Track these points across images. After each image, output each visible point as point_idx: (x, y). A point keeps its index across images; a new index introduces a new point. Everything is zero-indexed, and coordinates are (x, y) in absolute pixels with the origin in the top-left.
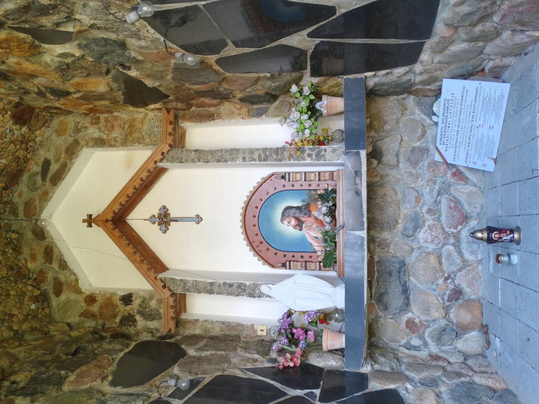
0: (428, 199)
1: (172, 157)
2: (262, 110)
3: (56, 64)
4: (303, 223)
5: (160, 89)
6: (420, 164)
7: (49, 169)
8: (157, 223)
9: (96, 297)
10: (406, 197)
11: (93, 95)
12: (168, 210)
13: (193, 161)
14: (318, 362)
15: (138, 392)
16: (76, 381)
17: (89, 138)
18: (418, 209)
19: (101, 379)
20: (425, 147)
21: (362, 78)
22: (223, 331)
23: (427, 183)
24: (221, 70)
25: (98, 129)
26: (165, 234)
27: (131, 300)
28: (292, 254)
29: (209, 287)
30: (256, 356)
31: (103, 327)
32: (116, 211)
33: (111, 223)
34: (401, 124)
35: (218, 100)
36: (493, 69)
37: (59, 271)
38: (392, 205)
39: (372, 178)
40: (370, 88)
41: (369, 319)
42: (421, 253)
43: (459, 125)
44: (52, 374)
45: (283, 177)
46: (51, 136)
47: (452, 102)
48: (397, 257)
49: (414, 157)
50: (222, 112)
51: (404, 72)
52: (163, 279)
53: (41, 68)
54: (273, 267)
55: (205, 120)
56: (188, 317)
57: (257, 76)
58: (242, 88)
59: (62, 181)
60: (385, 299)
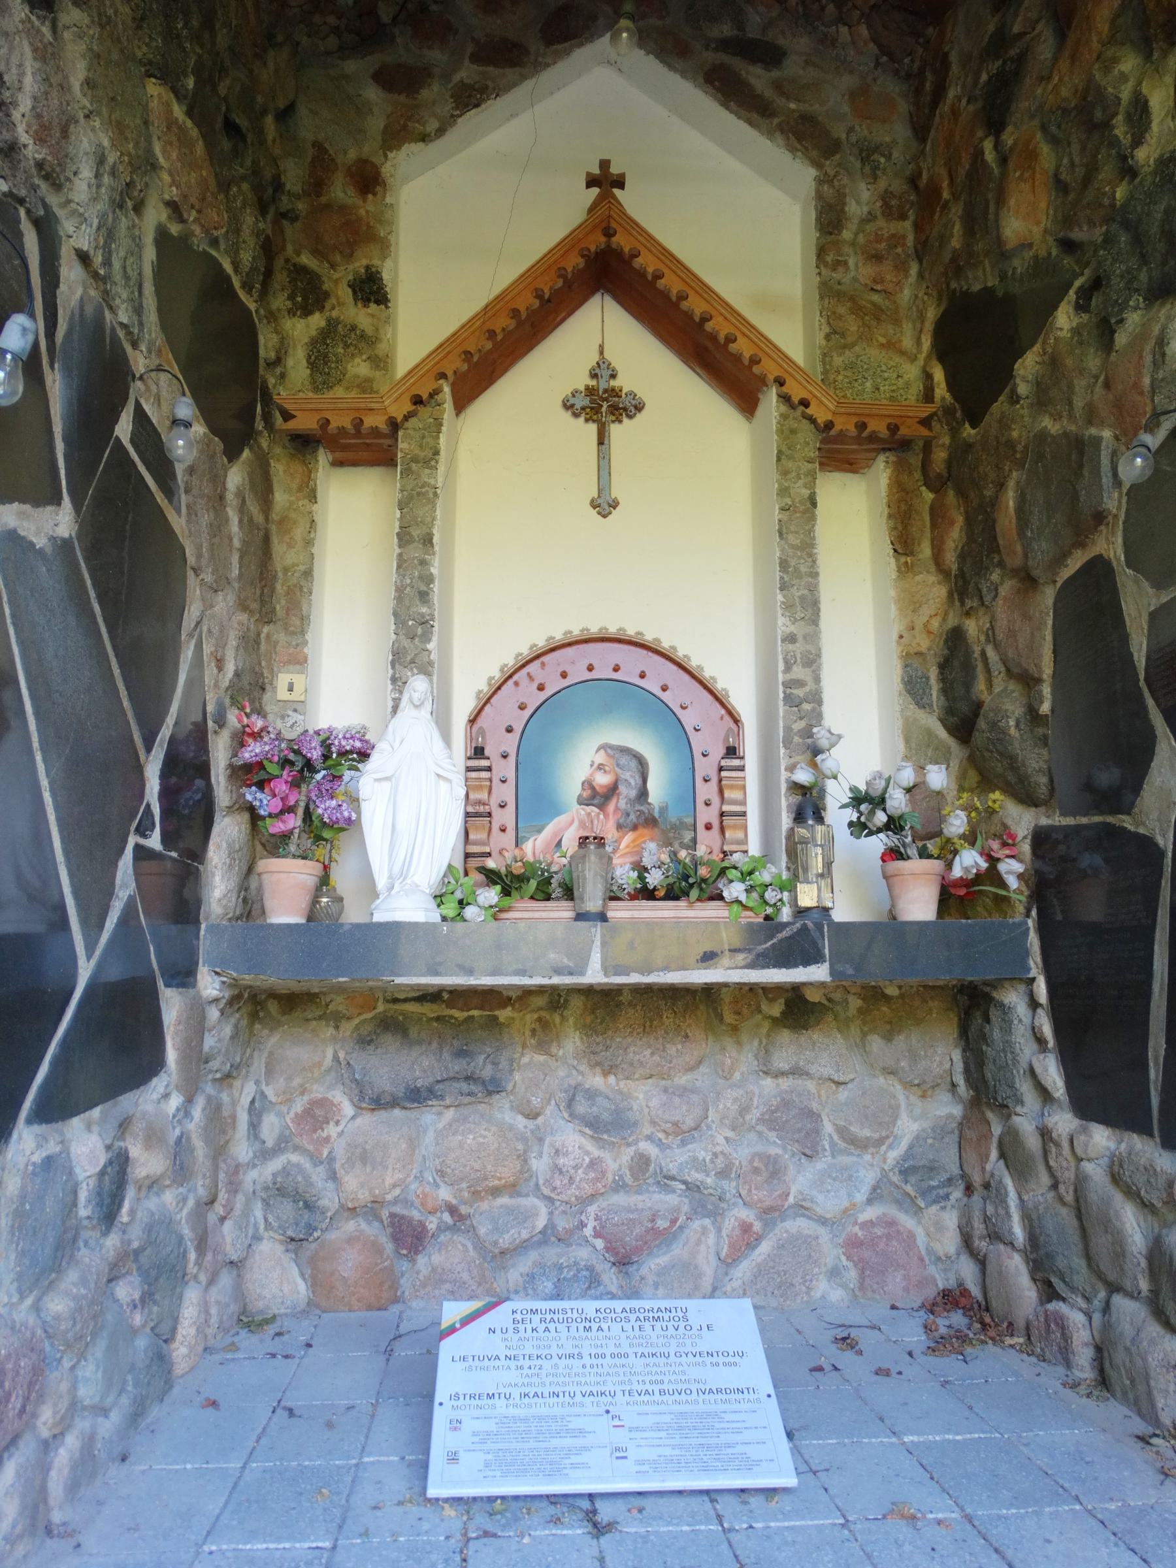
0: (676, 1159)
1: (793, 431)
2: (924, 693)
3: (1110, 90)
4: (602, 807)
5: (1001, 398)
6: (772, 1136)
7: (754, 60)
8: (593, 383)
9: (375, 194)
10: (679, 1096)
11: (987, 202)
12: (630, 417)
13: (783, 492)
14: (219, 847)
15: (146, 311)
16: (171, 123)
17: (844, 186)
18: (647, 1130)
19: (176, 199)
20: (820, 1148)
21: (1029, 970)
22: (285, 574)
23: (722, 1152)
24: (1066, 573)
25: (870, 213)
26: (560, 403)
27: (369, 300)
28: (511, 775)
29: (418, 532)
30: (230, 668)
31: (284, 215)
32: (638, 262)
33: (603, 246)
34: (882, 1080)
35: (954, 567)
36: (1057, 1324)
37: (451, 85)
38: (656, 1058)
39: (730, 1003)
40: (995, 994)
41: (333, 996)
42: (524, 1140)
43: (604, 1356)
44: (184, 50)
45: (731, 752)
46: (851, 72)
47: (681, 1328)
48: (511, 1071)
49: (794, 1117)
50: (918, 578)
51: (1048, 1084)
52: (439, 397)
53: (1095, 45)
54: (472, 721)
55: (896, 528)
56: (320, 470)
57: (1045, 677)
58: (1000, 636)
59: (719, 100)
60: (390, 1041)
